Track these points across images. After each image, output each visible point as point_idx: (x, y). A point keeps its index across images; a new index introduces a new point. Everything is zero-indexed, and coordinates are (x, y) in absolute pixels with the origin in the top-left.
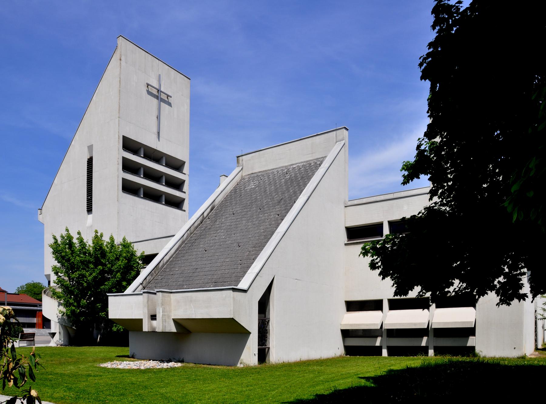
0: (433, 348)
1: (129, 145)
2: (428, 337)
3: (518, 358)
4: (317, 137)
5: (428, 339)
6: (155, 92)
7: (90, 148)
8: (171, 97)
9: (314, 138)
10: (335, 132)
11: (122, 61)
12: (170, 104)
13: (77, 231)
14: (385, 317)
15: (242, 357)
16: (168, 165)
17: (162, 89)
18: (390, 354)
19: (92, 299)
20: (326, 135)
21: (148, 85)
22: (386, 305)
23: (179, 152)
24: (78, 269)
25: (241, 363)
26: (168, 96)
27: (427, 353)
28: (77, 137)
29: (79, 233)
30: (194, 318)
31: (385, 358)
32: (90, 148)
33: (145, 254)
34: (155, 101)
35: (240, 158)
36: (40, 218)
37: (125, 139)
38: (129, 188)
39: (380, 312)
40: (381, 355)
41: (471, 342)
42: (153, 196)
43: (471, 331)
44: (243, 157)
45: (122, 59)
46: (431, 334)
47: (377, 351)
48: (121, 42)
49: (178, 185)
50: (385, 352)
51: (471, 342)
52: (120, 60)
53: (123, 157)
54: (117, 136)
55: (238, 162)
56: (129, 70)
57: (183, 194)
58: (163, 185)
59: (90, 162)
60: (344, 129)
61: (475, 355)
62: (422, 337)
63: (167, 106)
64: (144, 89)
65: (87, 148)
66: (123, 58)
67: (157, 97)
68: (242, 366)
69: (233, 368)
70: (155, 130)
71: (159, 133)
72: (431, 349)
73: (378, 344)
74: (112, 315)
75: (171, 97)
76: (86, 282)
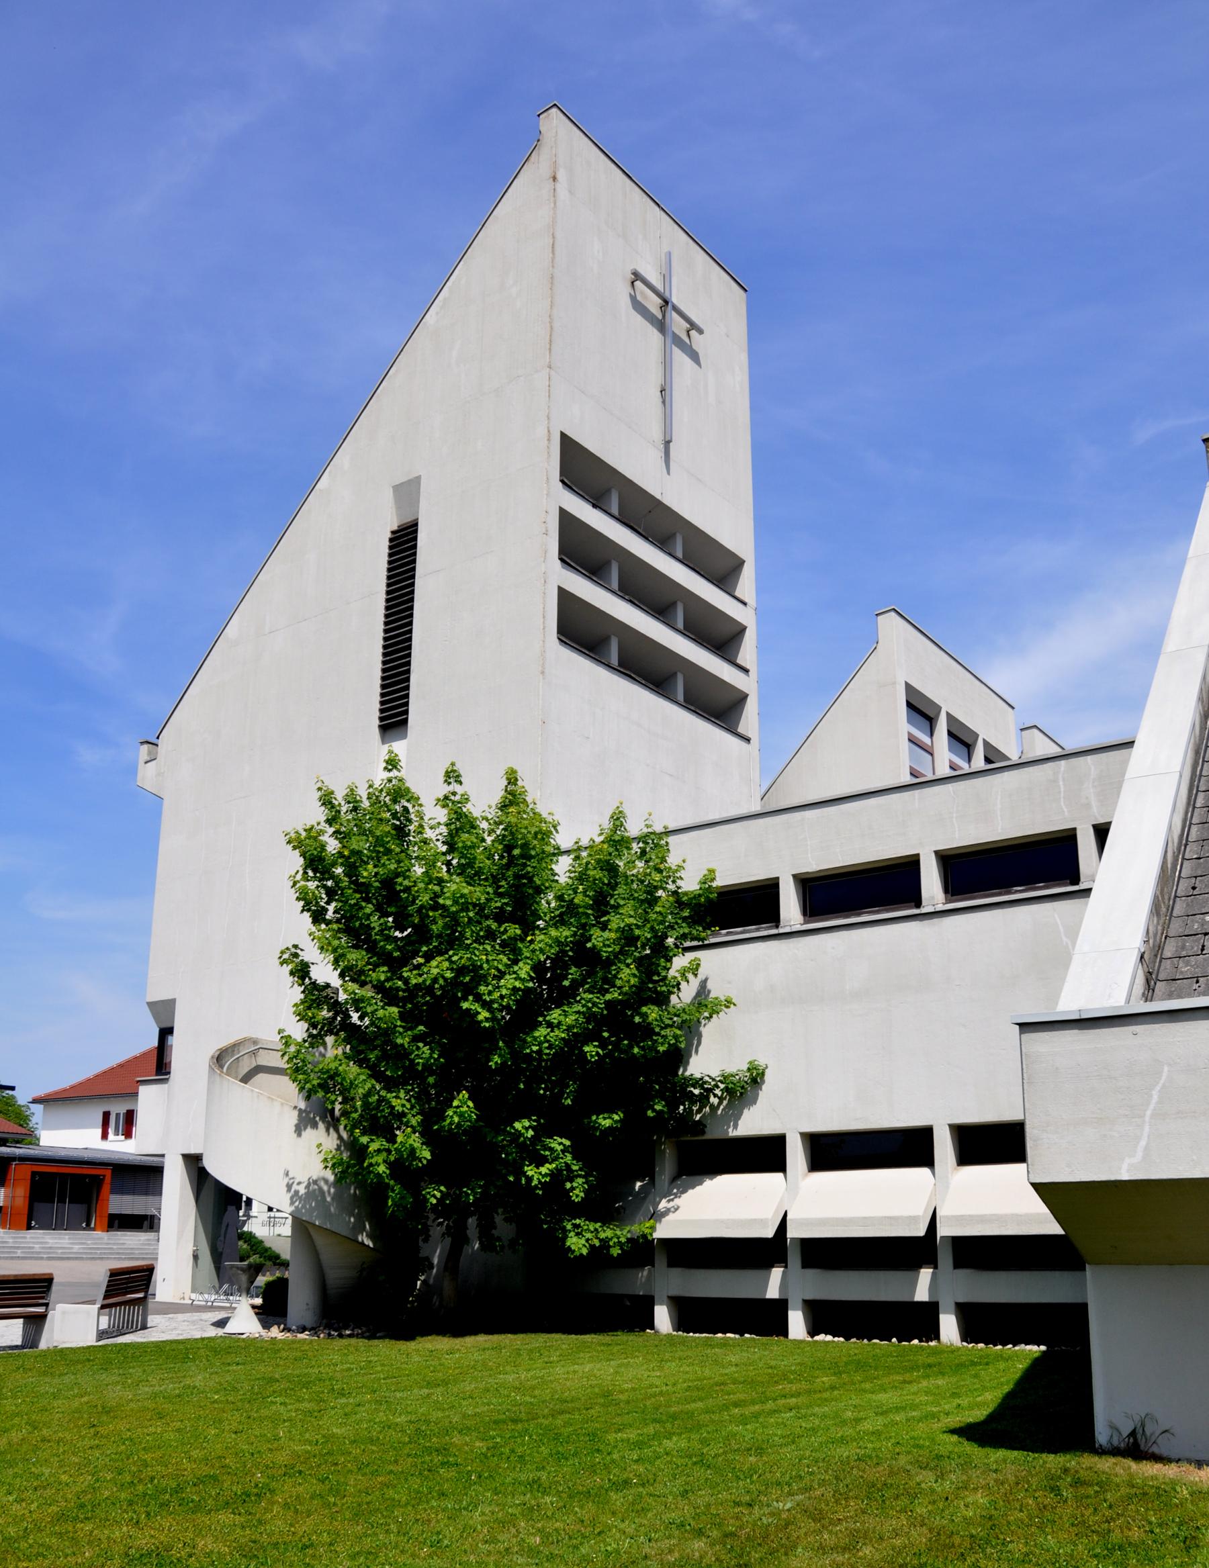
0: (953, 1307)
1: (581, 469)
5: (784, 1274)
6: (653, 304)
7: (408, 491)
8: (701, 332)
11: (558, 186)
12: (695, 357)
13: (446, 765)
16: (688, 562)
17: (675, 300)
18: (968, 1334)
19: (522, 1086)
21: (637, 276)
23: (728, 521)
24: (452, 941)
26: (693, 326)
27: (932, 1332)
28: (343, 459)
29: (452, 776)
31: (952, 1350)
32: (408, 491)
33: (719, 882)
34: (654, 335)
36: (148, 776)
37: (568, 445)
38: (581, 631)
39: (924, 1171)
40: (786, 1335)
42: (649, 670)
45: (559, 176)
46: (945, 1257)
47: (922, 1321)
48: (554, 125)
49: (723, 639)
50: (949, 1326)
52: (554, 179)
53: (562, 512)
54: (541, 431)
56: (572, 225)
57: (741, 675)
58: (609, 666)
59: (404, 544)
60: (893, 614)
63: (687, 360)
64: (624, 291)
65: (389, 495)
66: (561, 175)
67: (661, 326)
70: (657, 435)
71: (667, 443)
72: (946, 1312)
73: (922, 1294)
75: (701, 332)
76: (487, 1005)
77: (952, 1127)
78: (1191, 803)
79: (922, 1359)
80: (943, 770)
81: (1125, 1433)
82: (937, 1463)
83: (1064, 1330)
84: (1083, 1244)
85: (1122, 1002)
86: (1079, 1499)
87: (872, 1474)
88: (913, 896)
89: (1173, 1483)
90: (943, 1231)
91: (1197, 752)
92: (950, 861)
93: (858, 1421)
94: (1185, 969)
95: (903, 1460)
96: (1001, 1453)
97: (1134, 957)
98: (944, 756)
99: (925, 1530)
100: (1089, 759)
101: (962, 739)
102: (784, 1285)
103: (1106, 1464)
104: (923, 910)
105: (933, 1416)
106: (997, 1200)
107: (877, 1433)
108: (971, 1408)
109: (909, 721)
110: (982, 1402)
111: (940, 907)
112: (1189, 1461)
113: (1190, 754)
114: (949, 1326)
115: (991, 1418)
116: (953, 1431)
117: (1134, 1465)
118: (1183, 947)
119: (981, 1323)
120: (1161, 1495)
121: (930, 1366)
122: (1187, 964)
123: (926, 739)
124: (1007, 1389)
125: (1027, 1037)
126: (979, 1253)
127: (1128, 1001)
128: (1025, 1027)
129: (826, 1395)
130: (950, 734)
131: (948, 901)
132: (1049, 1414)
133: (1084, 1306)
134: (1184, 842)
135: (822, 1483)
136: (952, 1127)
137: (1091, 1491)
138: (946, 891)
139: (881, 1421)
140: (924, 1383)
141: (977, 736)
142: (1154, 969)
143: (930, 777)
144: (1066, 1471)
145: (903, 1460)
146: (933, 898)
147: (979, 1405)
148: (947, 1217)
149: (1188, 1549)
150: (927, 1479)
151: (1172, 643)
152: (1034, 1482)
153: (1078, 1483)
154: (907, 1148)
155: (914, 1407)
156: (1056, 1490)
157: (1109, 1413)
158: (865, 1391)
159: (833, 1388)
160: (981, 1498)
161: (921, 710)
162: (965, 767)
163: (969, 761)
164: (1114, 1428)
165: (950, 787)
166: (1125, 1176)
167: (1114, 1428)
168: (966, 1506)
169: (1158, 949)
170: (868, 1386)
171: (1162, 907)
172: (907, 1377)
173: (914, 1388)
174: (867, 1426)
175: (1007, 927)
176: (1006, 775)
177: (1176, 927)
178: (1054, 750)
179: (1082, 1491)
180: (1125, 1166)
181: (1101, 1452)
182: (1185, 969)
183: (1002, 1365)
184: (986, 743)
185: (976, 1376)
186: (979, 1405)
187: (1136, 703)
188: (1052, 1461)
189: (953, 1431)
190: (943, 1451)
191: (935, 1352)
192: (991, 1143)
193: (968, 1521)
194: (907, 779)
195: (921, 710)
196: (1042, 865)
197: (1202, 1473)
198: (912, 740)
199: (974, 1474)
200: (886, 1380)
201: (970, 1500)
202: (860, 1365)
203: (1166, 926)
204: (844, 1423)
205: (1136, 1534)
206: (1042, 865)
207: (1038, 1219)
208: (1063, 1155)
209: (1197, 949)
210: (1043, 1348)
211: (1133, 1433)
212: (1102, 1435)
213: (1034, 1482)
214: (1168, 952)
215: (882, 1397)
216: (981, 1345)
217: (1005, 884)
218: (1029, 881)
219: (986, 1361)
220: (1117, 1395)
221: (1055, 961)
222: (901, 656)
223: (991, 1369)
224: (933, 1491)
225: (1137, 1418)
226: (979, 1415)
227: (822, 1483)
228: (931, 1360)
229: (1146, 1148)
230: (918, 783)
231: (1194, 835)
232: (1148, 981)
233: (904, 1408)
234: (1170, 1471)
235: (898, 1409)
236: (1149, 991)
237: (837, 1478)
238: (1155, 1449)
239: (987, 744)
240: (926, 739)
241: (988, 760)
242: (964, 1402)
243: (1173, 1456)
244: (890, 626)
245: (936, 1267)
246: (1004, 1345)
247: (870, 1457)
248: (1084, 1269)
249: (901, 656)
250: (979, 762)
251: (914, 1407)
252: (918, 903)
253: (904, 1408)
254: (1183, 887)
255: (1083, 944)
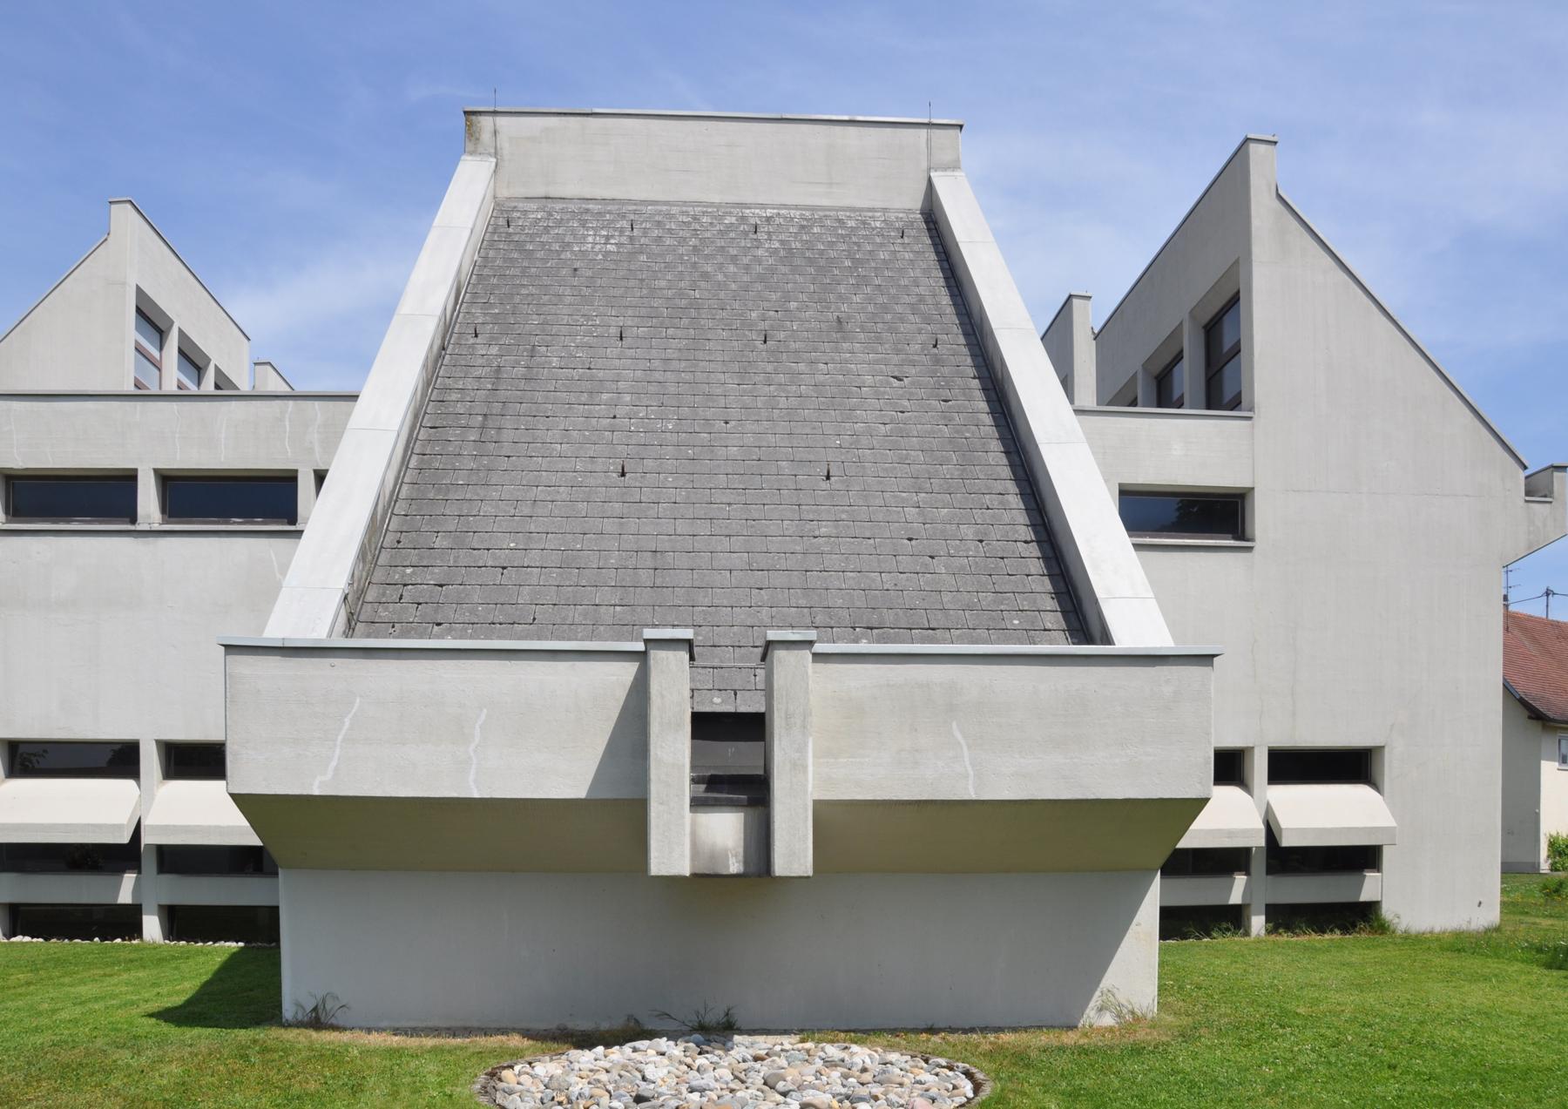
0: (156, 908)
2: (1248, 873)
3: (1487, 930)
4: (852, 130)
5: (137, 880)
9: (838, 129)
10: (923, 132)
14: (146, 800)
15: (1106, 983)
20: (888, 131)
22: (150, 761)
25: (1100, 1010)
27: (135, 930)
30: (972, 795)
31: (155, 947)
35: (486, 123)
39: (131, 783)
41: (1371, 887)
43: (1364, 858)
44: (502, 121)
46: (149, 863)
47: (125, 922)
50: (152, 926)
51: (1371, 887)
55: (470, 126)
60: (129, 206)
61: (1382, 928)
62: (122, 871)
68: (1108, 1020)
69: (1069, 1038)
73: (125, 896)
74: (1543, 763)
77: (158, 742)
78: (405, 462)
79: (123, 955)
80: (170, 387)
81: (309, 1009)
82: (134, 1043)
83: (258, 928)
84: (275, 852)
85: (324, 635)
86: (265, 1063)
87: (65, 1056)
88: (128, 512)
89: (347, 1046)
90: (147, 839)
91: (416, 416)
92: (169, 482)
93: (54, 1011)
94: (384, 614)
95: (100, 1043)
96: (197, 1031)
97: (338, 597)
98: (173, 375)
99: (119, 1100)
100: (317, 404)
101: (193, 361)
102: (1248, 889)
103: (290, 1035)
104: (138, 527)
105: (132, 1003)
106: (201, 812)
107: (75, 1021)
108: (169, 995)
109: (137, 328)
110: (183, 985)
111: (156, 527)
112: (361, 1029)
113: (410, 417)
114: (152, 926)
115: (189, 1002)
116: (151, 1015)
117: (314, 1034)
118: (384, 595)
119: (181, 923)
120: (336, 1056)
121: (131, 961)
122: (386, 609)
123: (155, 352)
124: (205, 978)
125: (232, 658)
126: (181, 860)
127: (330, 635)
128: (230, 649)
129: (23, 990)
130: (181, 352)
131: (164, 522)
132: (244, 998)
133: (276, 909)
134: (394, 498)
135: (13, 1069)
136: (158, 742)
137: (276, 1056)
138: (163, 511)
139: (78, 1010)
140: (125, 976)
141: (172, 323)
142: (355, 609)
143: (154, 390)
144: (255, 1042)
145: (100, 1043)
146: (149, 516)
147: (178, 993)
148: (153, 827)
149: (354, 1093)
150: (124, 1056)
151: (406, 307)
152: (226, 1052)
153: (265, 1050)
154: (118, 760)
155: (113, 996)
156: (245, 1058)
157: (294, 992)
158: (63, 985)
159: (28, 984)
160: (175, 1069)
161: (151, 320)
162: (193, 389)
163: (199, 384)
164: (298, 1005)
165: (175, 406)
166: (316, 792)
167: (298, 1005)
168: (161, 1076)
169: (361, 593)
170: (67, 980)
171: (368, 554)
172: (108, 971)
173: (115, 980)
174: (64, 1015)
175: (218, 557)
176: (234, 404)
177: (379, 576)
178: (283, 389)
179: (268, 1056)
180: (316, 783)
181: (288, 1025)
182: (384, 614)
183: (202, 959)
184: (218, 371)
185: (176, 968)
186: (178, 993)
187: (364, 362)
188: (243, 1035)
189: (151, 1015)
190: (140, 1032)
191: (137, 949)
192: (195, 760)
193: (162, 1089)
194: (131, 389)
195: (151, 320)
196: (261, 500)
197: (370, 1037)
198: (139, 350)
199: (169, 1049)
200: (86, 974)
201: (165, 1071)
202: (59, 962)
203: (370, 573)
204: (40, 1014)
205: (312, 1086)
206: (261, 500)
207: (235, 829)
208: (255, 771)
209: (396, 598)
210: (241, 944)
211: (315, 1009)
212: (288, 1011)
213: (226, 1052)
214: (369, 598)
215: (82, 989)
216: (183, 943)
217: (224, 514)
218: (248, 514)
219: (187, 956)
220: (301, 975)
221: (265, 594)
222: (132, 256)
223: (191, 962)
224: (129, 1066)
225: (319, 997)
226: (178, 1000)
227: (13, 1069)
228: (132, 956)
229: (337, 769)
230: (140, 395)
231: (403, 494)
232: (349, 621)
233: (103, 998)
234: (345, 1037)
235: (96, 999)
236: (350, 629)
237: (29, 1063)
238: (333, 1021)
239: (218, 371)
240: (155, 352)
241: (217, 387)
242: (164, 990)
243: (348, 1025)
244: (124, 220)
245: (139, 872)
246: (205, 941)
247: (66, 1042)
248: (276, 874)
249: (132, 256)
250: (208, 385)
251: (113, 996)
252: (133, 519)
253: (103, 998)
254: (389, 540)
255: (292, 579)
